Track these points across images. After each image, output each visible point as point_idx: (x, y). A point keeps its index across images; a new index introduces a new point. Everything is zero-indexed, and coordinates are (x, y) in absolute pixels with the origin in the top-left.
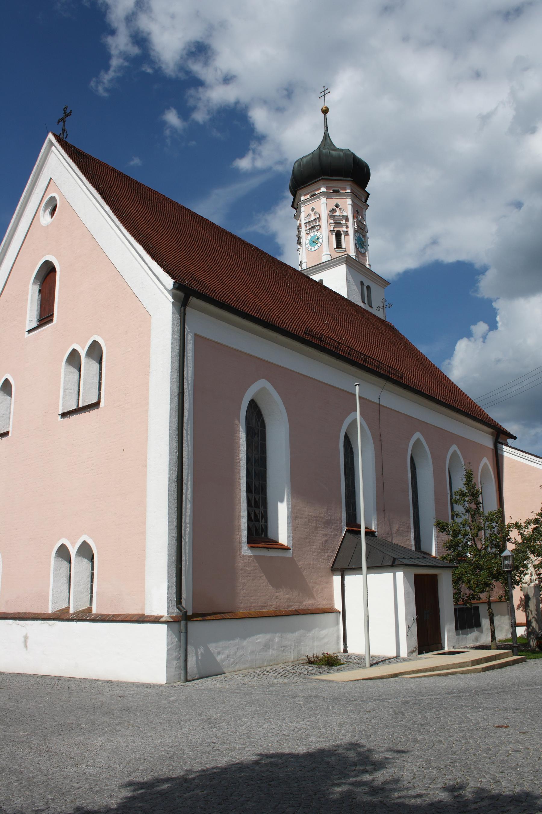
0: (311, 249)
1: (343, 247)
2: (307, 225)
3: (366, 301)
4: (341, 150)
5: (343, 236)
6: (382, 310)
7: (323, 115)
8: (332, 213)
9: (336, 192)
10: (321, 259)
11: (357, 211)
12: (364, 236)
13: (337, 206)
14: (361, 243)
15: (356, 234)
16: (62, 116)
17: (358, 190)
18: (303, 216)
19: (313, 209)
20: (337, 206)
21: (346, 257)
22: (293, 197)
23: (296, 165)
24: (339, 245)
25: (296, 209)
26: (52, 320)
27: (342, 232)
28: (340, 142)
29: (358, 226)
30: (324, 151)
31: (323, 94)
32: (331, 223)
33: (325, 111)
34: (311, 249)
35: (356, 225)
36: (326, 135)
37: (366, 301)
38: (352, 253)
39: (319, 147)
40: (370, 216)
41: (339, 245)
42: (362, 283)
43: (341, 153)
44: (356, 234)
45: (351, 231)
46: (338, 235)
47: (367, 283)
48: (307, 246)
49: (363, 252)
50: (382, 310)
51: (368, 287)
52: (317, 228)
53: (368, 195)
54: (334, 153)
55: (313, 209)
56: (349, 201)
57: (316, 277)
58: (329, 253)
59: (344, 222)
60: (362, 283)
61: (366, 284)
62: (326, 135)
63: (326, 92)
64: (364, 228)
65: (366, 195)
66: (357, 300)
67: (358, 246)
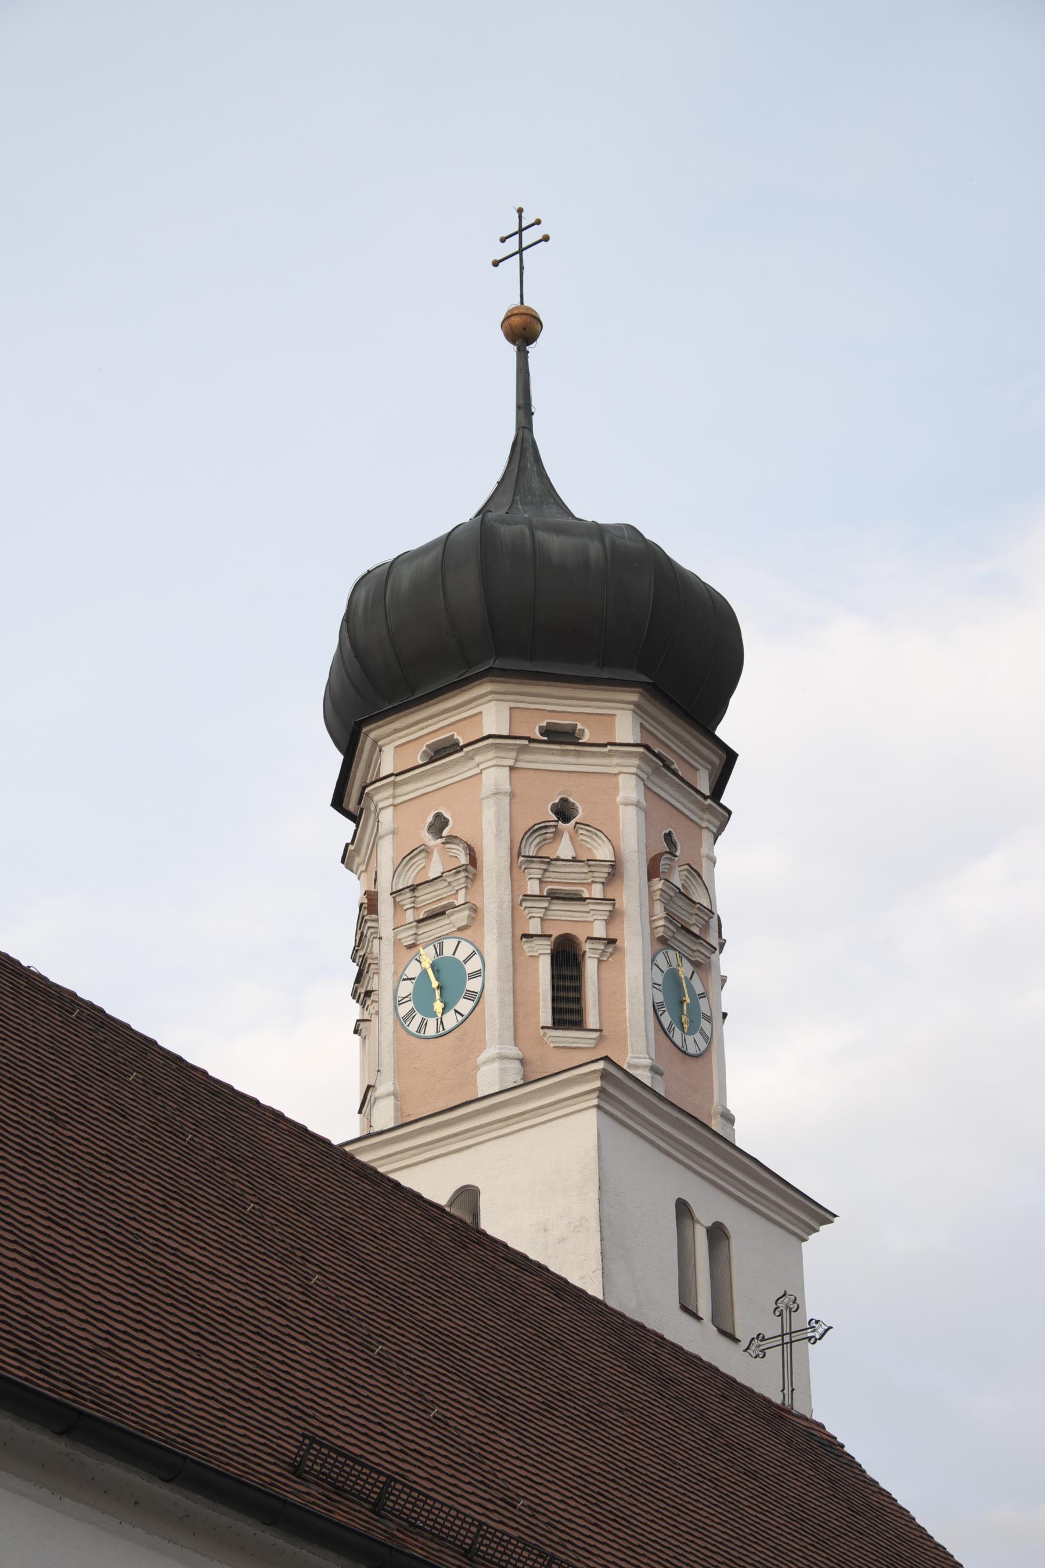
0: (423, 1024)
1: (592, 1019)
2: (406, 899)
3: (704, 1307)
4: (598, 531)
5: (590, 967)
6: (774, 1355)
7: (511, 350)
8: (529, 849)
9: (560, 736)
10: (472, 1081)
11: (668, 837)
12: (703, 966)
13: (564, 811)
14: (686, 1009)
15: (661, 959)
16: (517, 229)
17: (676, 739)
18: (386, 854)
19: (439, 824)
20: (564, 811)
21: (604, 1075)
22: (340, 758)
23: (362, 593)
24: (568, 1011)
25: (354, 818)
26: (737, 755)
27: (587, 947)
28: (592, 490)
29: (670, 917)
30: (505, 530)
31: (513, 244)
32: (527, 897)
33: (522, 330)
34: (423, 1024)
35: (659, 909)
36: (524, 453)
37: (704, 1307)
38: (637, 1054)
39: (483, 511)
40: (742, 868)
41: (568, 1011)
42: (683, 1209)
43: (594, 548)
44: (661, 959)
45: (635, 944)
46: (566, 957)
47: (710, 1206)
48: (403, 1010)
49: (692, 1050)
50: (774, 1355)
51: (717, 1234)
52: (460, 918)
53: (730, 757)
54: (554, 543)
55: (439, 824)
56: (629, 788)
57: (433, 1182)
58: (514, 1051)
59: (597, 891)
60: (683, 1209)
61: (705, 1215)
62: (524, 453)
63: (529, 237)
64: (706, 926)
65: (717, 761)
66: (650, 1300)
67: (666, 1019)
